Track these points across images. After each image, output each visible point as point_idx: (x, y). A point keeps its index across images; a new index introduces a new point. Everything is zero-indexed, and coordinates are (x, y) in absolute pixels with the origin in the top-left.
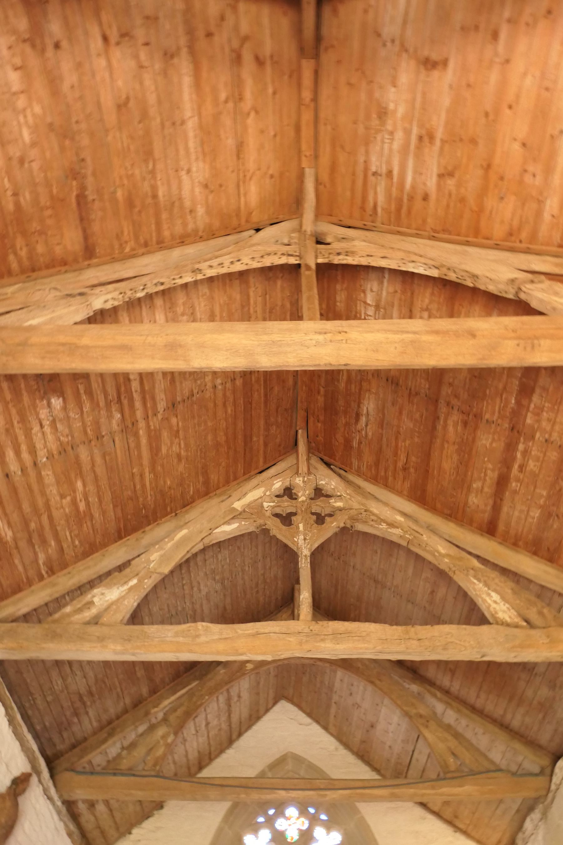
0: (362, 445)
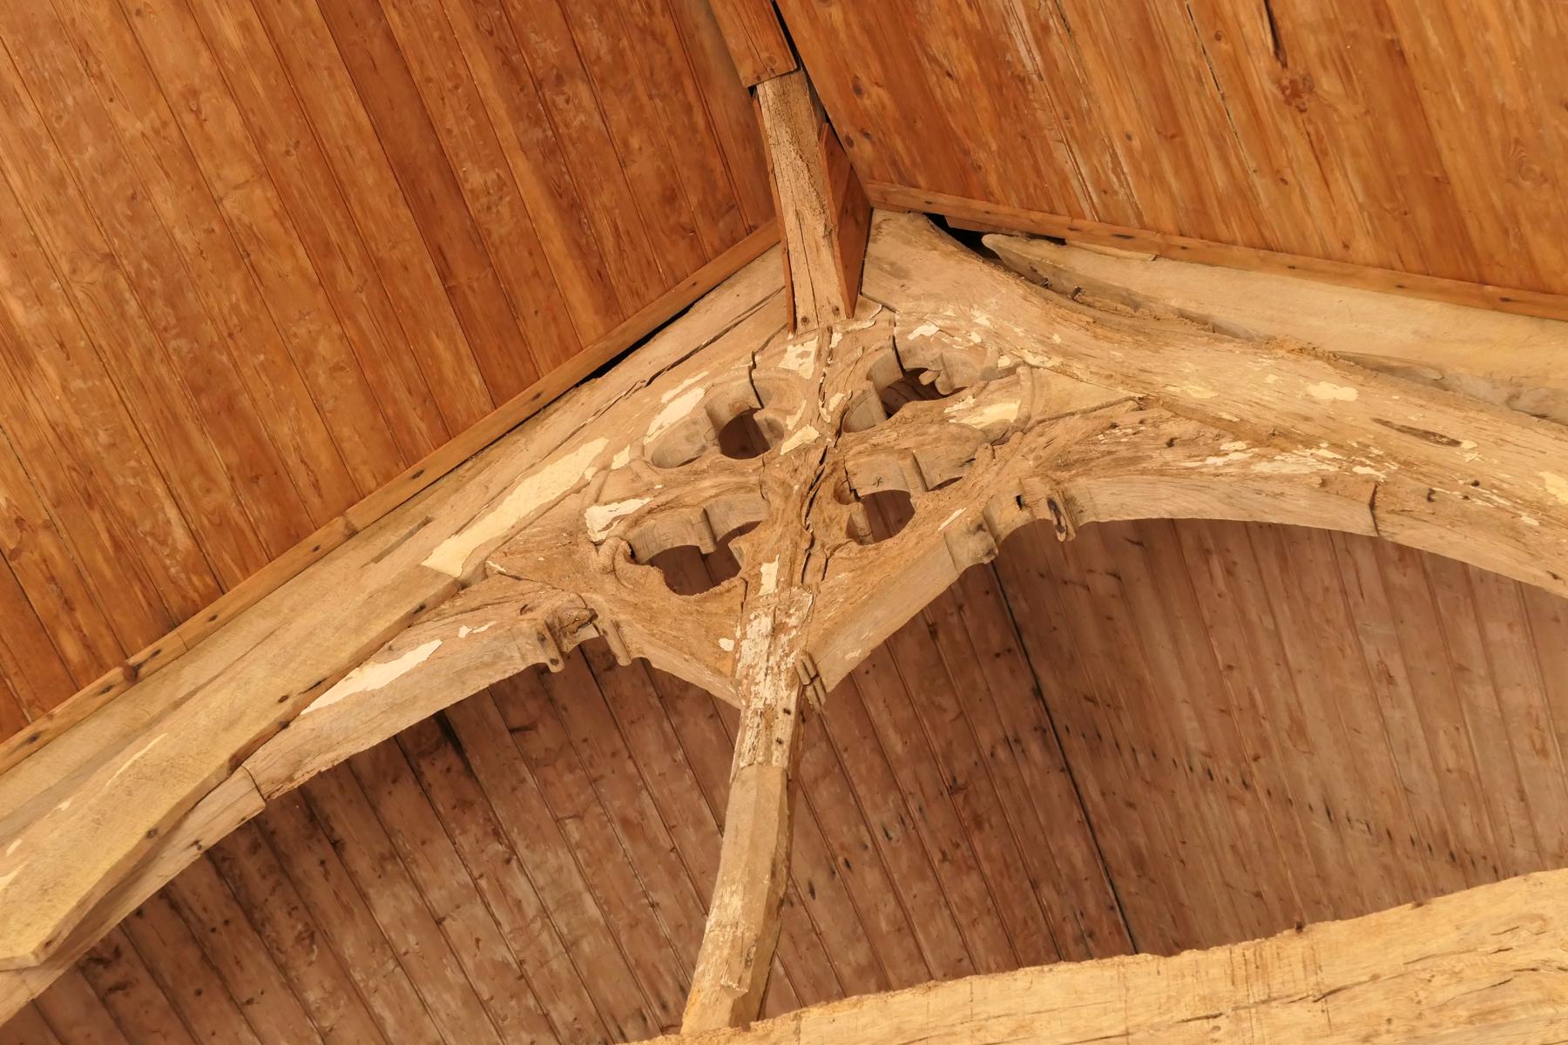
0: (1055, 38)
